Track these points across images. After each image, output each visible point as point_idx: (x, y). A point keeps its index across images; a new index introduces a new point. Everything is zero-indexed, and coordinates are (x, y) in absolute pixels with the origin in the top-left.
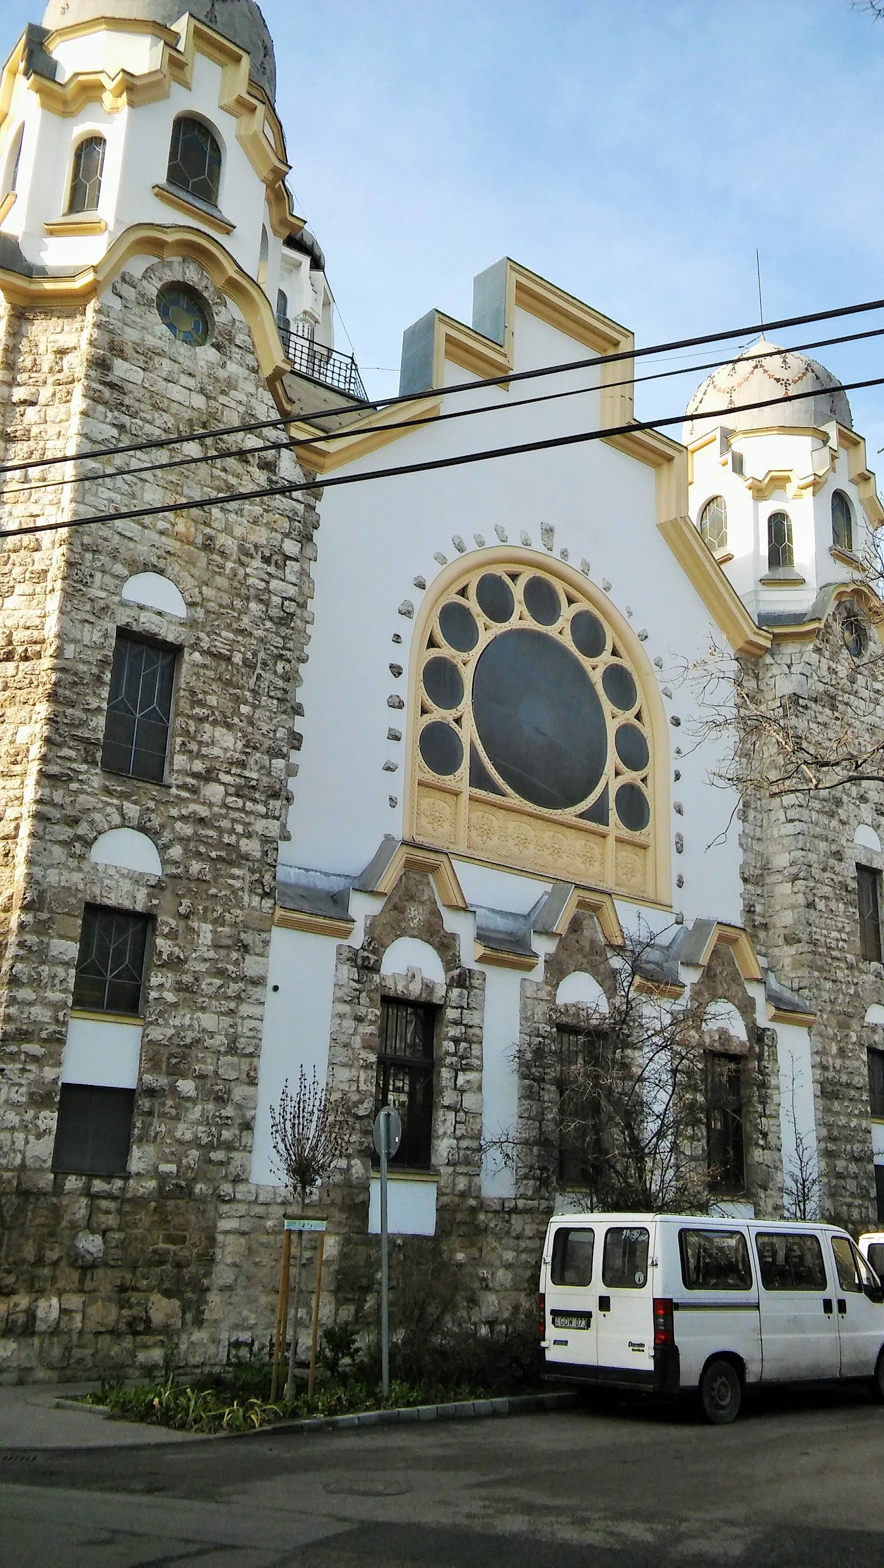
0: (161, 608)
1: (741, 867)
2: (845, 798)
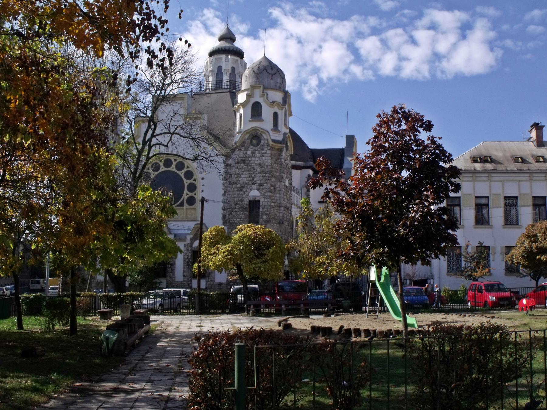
0: (440, 136)
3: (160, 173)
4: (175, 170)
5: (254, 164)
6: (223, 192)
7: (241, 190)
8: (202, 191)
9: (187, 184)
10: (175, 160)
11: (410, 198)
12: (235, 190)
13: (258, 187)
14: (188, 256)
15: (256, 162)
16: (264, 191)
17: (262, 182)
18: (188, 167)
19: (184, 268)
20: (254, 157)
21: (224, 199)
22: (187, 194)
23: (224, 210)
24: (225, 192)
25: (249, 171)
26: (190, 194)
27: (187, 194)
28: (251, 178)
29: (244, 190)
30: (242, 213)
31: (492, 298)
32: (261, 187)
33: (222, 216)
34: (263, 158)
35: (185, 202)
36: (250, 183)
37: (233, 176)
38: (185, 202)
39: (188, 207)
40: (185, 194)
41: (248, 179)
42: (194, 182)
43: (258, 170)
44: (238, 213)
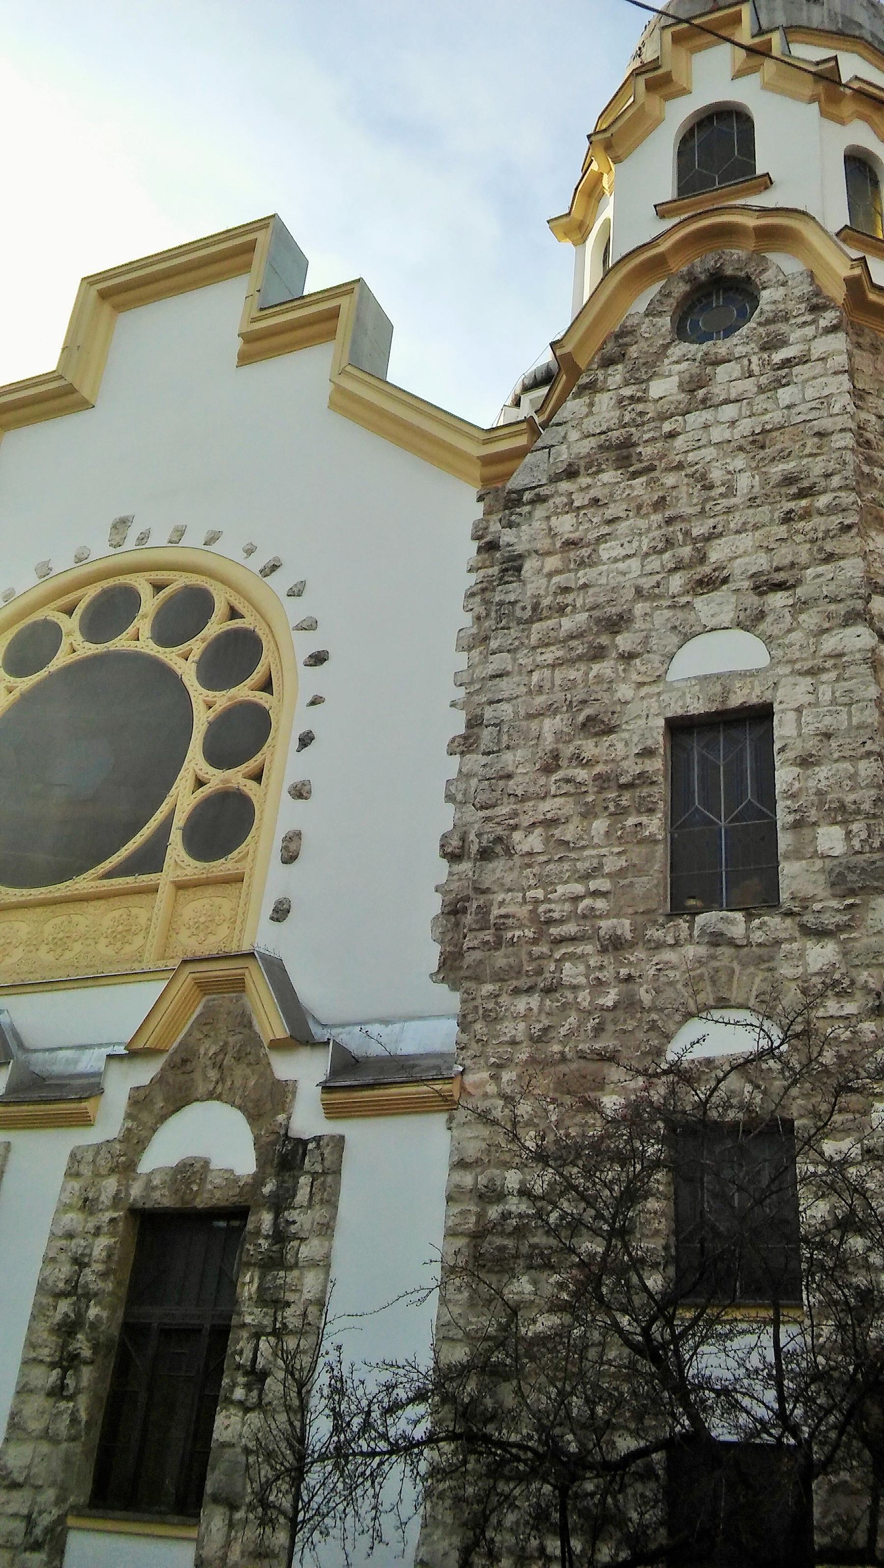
1: (444, 837)
2: (640, 608)
3: (51, 675)
4: (148, 646)
5: (709, 453)
6: (457, 724)
7: (598, 654)
8: (306, 740)
9: (211, 715)
10: (158, 587)
11: (482, 1499)
12: (550, 655)
13: (753, 600)
14: (80, 1262)
15: (718, 434)
16: (810, 619)
17: (784, 555)
18: (234, 614)
19: (24, 1390)
20: (705, 403)
21: (464, 775)
22: (200, 783)
23: (454, 857)
24: (474, 723)
25: (660, 504)
26: (217, 779)
27: (200, 783)
28: (686, 551)
29: (624, 641)
30: (600, 825)
31: (805, 1500)
32: (778, 600)
33: (435, 904)
34: (785, 395)
35: (176, 837)
36: (676, 582)
37: (530, 566)
38: (176, 837)
39: (193, 868)
40: (182, 786)
41: (654, 563)
42: (261, 698)
43: (743, 482)
44: (569, 832)
